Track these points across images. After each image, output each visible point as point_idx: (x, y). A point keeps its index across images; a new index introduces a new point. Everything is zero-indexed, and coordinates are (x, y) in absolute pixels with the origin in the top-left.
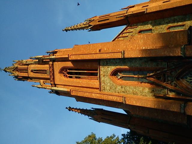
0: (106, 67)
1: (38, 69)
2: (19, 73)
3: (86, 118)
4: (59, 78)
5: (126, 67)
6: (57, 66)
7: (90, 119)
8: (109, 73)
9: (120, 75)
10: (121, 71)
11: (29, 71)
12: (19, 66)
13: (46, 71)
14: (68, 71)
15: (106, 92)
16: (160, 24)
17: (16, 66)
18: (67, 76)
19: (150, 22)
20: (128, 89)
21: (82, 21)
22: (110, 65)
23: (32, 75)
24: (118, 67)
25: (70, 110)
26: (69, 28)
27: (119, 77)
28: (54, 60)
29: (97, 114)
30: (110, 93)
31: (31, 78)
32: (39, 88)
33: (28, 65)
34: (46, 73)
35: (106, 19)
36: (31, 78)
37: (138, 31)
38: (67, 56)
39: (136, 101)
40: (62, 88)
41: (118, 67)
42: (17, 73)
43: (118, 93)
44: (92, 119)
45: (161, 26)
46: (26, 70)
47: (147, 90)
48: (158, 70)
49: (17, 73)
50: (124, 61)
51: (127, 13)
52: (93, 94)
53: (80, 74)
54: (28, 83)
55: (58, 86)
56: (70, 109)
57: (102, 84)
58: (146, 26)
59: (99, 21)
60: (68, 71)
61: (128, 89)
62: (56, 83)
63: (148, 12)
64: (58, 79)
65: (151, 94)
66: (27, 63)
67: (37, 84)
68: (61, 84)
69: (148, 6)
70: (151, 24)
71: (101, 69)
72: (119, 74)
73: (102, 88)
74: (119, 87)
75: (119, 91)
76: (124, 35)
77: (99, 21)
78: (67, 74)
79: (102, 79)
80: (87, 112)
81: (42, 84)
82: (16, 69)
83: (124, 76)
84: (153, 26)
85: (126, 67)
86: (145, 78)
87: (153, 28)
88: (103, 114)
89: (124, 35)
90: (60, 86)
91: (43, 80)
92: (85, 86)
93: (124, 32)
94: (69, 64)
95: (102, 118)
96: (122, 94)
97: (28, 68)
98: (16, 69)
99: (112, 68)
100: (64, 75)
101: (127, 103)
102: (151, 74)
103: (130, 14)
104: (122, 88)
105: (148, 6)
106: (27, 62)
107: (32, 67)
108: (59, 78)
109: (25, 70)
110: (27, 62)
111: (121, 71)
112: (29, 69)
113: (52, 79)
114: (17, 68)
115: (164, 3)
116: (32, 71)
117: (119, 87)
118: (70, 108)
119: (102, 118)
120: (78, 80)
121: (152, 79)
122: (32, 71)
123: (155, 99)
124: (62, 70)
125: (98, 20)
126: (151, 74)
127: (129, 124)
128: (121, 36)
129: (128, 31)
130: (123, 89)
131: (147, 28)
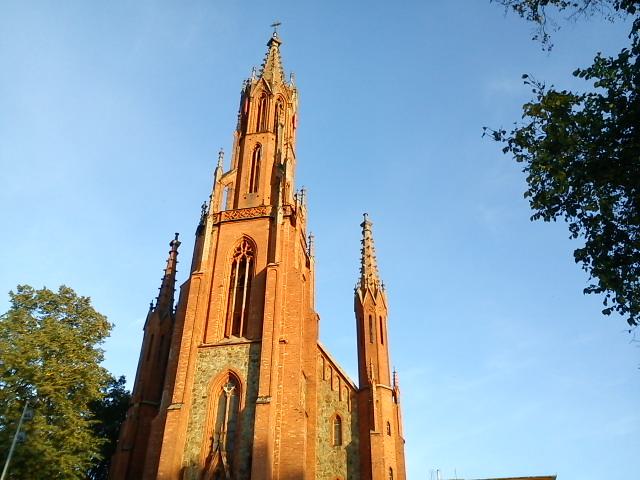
0: (247, 360)
1: (262, 169)
2: (258, 102)
3: (154, 293)
4: (233, 234)
5: (243, 406)
6: (259, 229)
7: (152, 304)
8: (234, 367)
9: (230, 393)
10: (237, 392)
11: (259, 138)
12: (273, 101)
13: (256, 190)
14: (248, 260)
15: (195, 360)
16: (349, 462)
17: (276, 91)
18: (238, 255)
19: (357, 441)
20: (201, 411)
21: (381, 272)
22: (249, 368)
23: (250, 145)
24: (245, 387)
25: (171, 244)
26: (367, 233)
27: (226, 389)
28: (273, 219)
29: (161, 324)
30: (193, 371)
31: (241, 142)
32: (215, 174)
33: (276, 132)
34: (251, 191)
35: (374, 337)
36: (241, 142)
37: (340, 413)
38: (277, 260)
39: (172, 432)
40: (207, 259)
41: (245, 387)
42: (256, 94)
43: (194, 390)
44: (151, 308)
45: (346, 466)
46: (261, 128)
47: (196, 451)
48: (231, 473)
49: (256, 94)
50: (253, 400)
51: (377, 387)
52: (190, 333)
53: (241, 289)
54: (232, 135)
55: (215, 233)
56: (175, 245)
57: (212, 351)
58: (350, 433)
59: (370, 317)
60: (248, 260)
61: (201, 411)
62: (222, 226)
63: (372, 437)
64: (230, 234)
65: (188, 460)
66: (279, 127)
67: (227, 163)
68: (220, 242)
69: (389, 434)
70: (352, 443)
71: (245, 346)
72: (233, 388)
73: (204, 350)
74: (203, 390)
75: (196, 392)
76: (336, 380)
77: (370, 317)
78: (241, 256)
79: (223, 351)
80: (166, 296)
81: (224, 180)
82: (267, 94)
83: (229, 399)
84: (347, 448)
85: (243, 406)
86: (219, 448)
87: (342, 447)
88: (163, 337)
89: (336, 380)
90: (215, 238)
91: (235, 181)
92: (211, 307)
93: (342, 380)
94: (261, 264)
95: (153, 336)
96: (189, 400)
97: (267, 132)
98: (267, 94)
99: (244, 376)
100: (239, 249)
101: (169, 414)
102: (224, 460)
103: (375, 395)
104: (204, 397)
105: (389, 434)
106: (282, 126)
107: (269, 148)
108: (233, 234)
109: (263, 123)
110: (282, 126)
111: (237, 392)
112: (263, 135)
113: (236, 216)
114: (271, 95)
115: (388, 472)
116: (258, 146)
117: (205, 390)
118: (178, 244)
119: (153, 336)
120: (226, 289)
121: (215, 462)
122: (258, 146)
123: (174, 470)
124: (249, 242)
125: (373, 315)
126: (224, 460)
127: (140, 404)
128: (335, 373)
129: (344, 389)
130: (200, 400)
131: (344, 435)
